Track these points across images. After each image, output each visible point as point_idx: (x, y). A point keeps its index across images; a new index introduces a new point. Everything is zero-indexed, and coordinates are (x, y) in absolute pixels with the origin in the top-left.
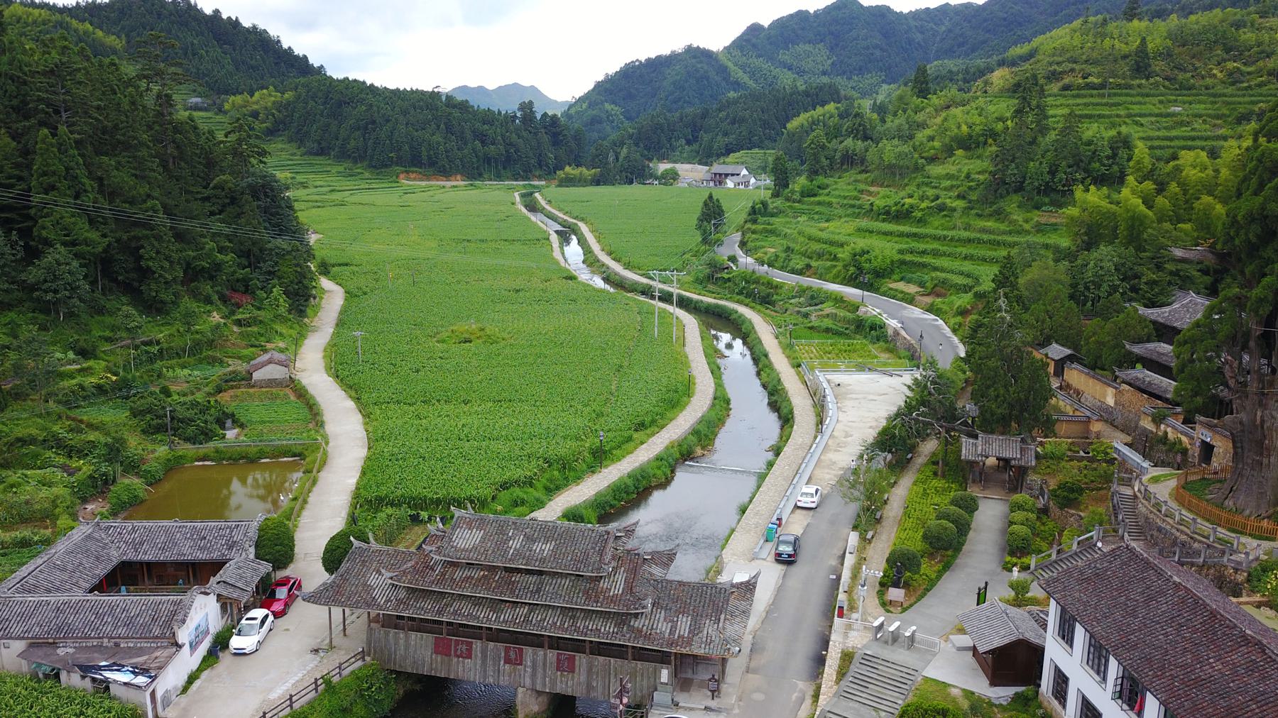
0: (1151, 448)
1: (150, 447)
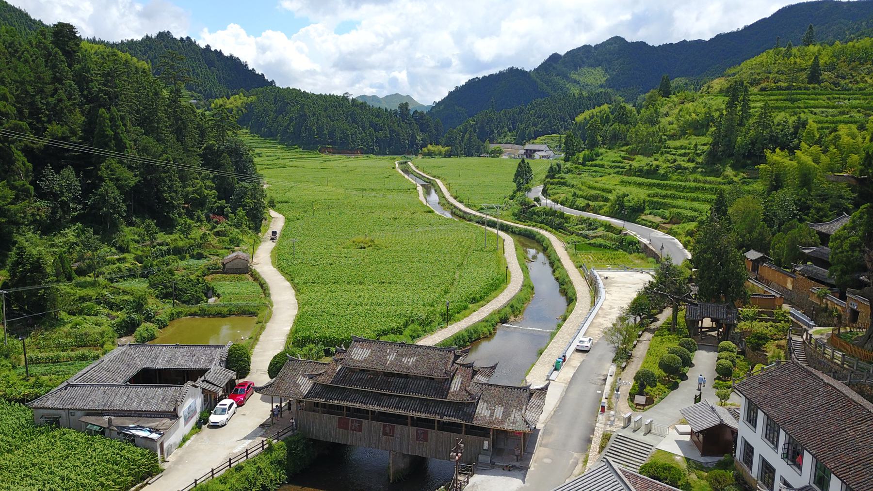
0: (816, 315)
1: (161, 306)
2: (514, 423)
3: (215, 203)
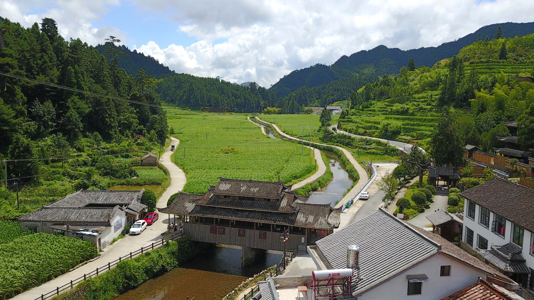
2: (321, 224)
3: (137, 127)
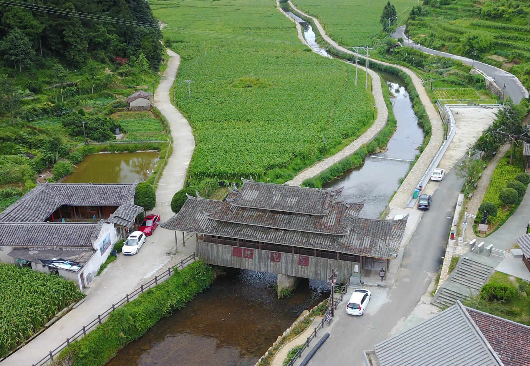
1: (74, 143)
